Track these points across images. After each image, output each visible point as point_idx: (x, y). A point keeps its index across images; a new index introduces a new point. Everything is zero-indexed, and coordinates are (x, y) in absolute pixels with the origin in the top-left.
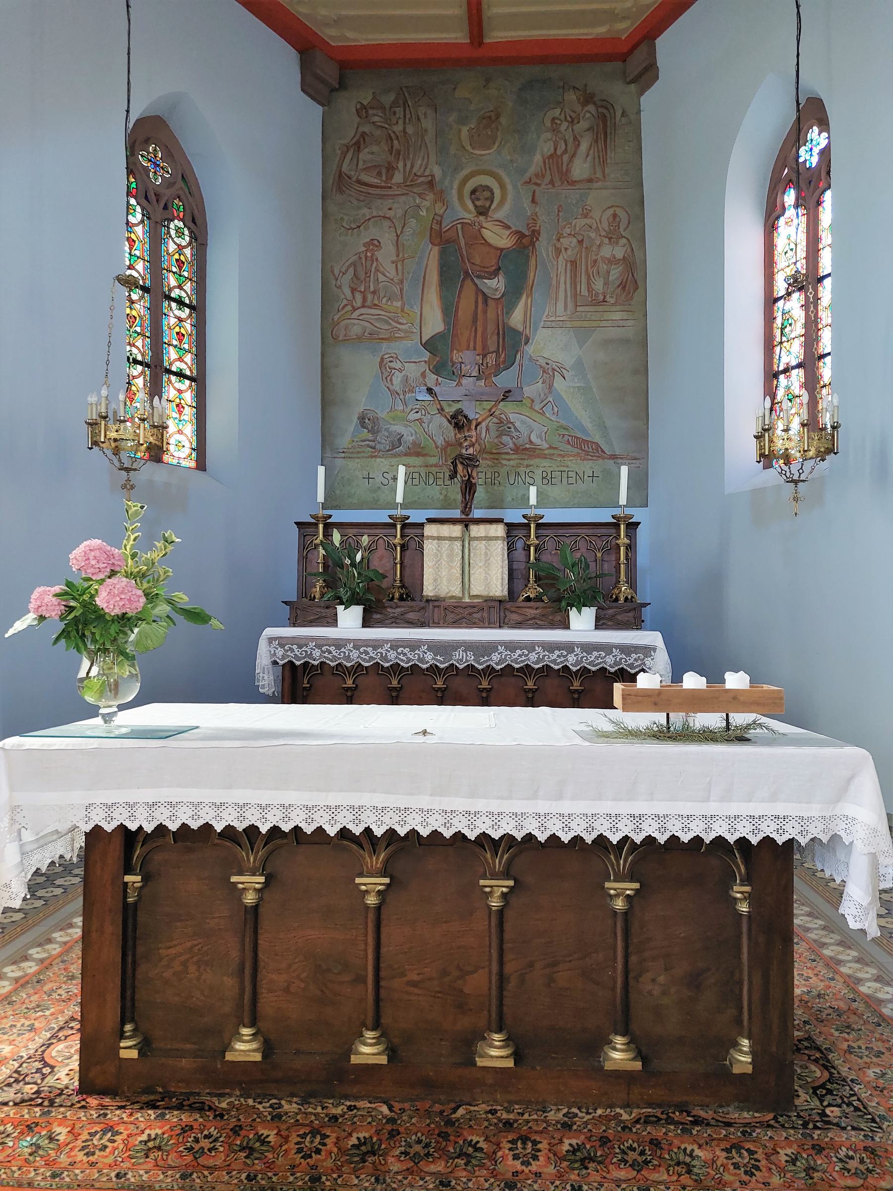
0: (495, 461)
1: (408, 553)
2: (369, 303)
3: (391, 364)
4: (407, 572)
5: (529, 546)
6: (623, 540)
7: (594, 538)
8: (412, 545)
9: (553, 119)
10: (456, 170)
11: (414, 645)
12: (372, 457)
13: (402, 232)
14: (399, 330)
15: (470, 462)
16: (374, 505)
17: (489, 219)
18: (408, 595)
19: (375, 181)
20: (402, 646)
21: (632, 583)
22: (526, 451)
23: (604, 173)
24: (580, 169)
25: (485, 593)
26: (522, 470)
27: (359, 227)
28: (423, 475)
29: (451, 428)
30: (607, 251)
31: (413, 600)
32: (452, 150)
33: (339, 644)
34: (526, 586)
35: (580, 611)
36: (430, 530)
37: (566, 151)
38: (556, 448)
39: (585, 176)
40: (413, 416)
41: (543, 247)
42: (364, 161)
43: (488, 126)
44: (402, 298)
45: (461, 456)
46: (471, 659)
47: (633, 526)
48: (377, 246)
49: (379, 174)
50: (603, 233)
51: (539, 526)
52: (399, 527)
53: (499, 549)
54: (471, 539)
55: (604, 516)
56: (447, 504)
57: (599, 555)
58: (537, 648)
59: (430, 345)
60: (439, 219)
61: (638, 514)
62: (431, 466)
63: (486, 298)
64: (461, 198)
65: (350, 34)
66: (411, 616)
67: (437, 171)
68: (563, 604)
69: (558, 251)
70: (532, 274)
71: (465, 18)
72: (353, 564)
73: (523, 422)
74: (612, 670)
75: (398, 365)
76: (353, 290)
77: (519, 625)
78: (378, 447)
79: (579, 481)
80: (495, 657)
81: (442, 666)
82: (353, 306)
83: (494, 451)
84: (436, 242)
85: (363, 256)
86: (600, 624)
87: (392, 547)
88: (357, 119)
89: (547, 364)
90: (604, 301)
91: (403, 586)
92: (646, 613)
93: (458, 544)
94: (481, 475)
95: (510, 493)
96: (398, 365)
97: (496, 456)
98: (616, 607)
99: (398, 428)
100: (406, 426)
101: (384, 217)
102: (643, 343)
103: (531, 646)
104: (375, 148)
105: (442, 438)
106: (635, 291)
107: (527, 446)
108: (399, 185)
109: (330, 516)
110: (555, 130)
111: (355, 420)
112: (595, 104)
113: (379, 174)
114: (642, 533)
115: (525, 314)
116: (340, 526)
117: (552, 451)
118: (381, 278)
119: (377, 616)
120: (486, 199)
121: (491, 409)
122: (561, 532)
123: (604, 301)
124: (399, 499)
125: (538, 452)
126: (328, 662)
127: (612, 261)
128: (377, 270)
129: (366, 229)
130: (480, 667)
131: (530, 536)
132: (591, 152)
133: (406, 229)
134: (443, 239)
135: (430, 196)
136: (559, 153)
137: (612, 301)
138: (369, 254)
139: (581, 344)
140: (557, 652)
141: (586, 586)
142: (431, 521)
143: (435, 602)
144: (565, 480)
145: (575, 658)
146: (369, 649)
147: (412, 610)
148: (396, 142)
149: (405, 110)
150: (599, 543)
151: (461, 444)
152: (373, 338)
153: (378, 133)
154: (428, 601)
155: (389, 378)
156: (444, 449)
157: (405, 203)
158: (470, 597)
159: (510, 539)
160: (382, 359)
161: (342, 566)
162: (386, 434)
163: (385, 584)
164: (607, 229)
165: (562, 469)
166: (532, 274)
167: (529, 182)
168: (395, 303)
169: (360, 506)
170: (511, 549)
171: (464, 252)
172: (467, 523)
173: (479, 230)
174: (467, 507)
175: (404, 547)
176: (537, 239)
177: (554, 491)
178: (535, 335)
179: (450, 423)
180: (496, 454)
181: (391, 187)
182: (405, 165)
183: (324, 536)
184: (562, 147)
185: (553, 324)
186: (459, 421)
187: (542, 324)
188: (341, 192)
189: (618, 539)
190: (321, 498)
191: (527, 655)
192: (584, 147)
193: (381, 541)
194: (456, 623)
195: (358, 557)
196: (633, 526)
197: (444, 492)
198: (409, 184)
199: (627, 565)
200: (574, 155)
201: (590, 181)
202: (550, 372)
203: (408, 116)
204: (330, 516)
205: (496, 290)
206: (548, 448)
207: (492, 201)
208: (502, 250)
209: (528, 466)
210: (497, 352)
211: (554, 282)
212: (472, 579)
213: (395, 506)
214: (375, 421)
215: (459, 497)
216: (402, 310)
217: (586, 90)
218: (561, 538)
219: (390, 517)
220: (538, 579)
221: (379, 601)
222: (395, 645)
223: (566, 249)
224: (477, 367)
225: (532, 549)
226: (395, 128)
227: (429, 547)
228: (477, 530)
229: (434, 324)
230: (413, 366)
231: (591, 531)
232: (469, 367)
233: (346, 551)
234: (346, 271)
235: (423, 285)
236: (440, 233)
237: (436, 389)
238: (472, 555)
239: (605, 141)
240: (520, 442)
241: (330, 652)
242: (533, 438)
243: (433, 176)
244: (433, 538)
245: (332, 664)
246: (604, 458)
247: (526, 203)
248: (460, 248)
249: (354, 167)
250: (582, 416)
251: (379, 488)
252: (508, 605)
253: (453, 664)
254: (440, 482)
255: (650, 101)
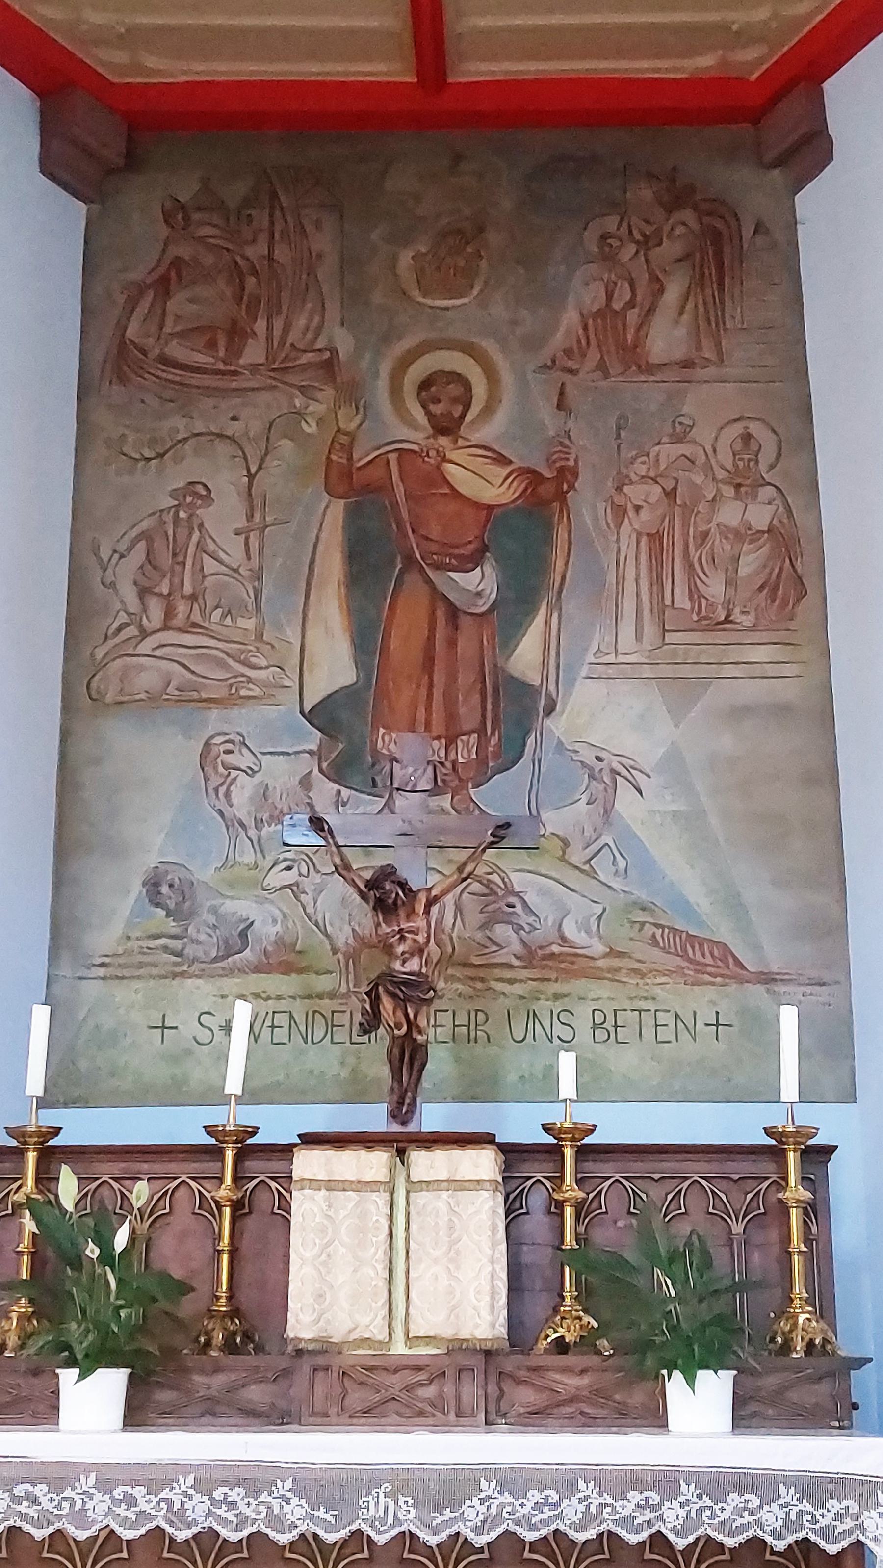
0: (479, 985)
1: (250, 1224)
2: (179, 620)
3: (229, 758)
4: (248, 1273)
5: (560, 1205)
6: (796, 1192)
7: (724, 1184)
8: (263, 1200)
9: (604, 237)
10: (387, 339)
11: (254, 1479)
12: (175, 976)
13: (260, 468)
14: (250, 680)
15: (413, 992)
16: (175, 1094)
17: (461, 442)
18: (247, 1337)
19: (201, 359)
20: (224, 1483)
21: (824, 1306)
22: (552, 961)
23: (718, 345)
24: (666, 338)
25: (448, 1332)
26: (543, 1007)
27: (161, 456)
28: (300, 1018)
29: (367, 908)
30: (730, 514)
31: (259, 1349)
32: (377, 298)
33: (59, 1476)
34: (556, 1311)
35: (691, 1381)
36: (308, 1164)
37: (631, 304)
38: (621, 955)
39: (679, 354)
40: (278, 878)
41: (587, 505)
42: (178, 317)
43: (458, 251)
44: (258, 609)
45: (388, 976)
46: (408, 1517)
47: (818, 1156)
48: (201, 497)
49: (212, 345)
50: (721, 474)
51: (585, 1152)
52: (229, 1155)
53: (486, 1211)
54: (413, 1186)
55: (744, 1125)
56: (356, 1092)
57: (738, 1228)
58: (582, 1485)
59: (324, 716)
60: (344, 439)
61: (827, 1123)
62: (320, 997)
63: (454, 613)
64: (396, 391)
65: (151, 62)
66: (256, 1394)
67: (345, 343)
68: (650, 1362)
69: (620, 513)
70: (560, 564)
71: (407, 38)
72: (107, 1257)
73: (542, 892)
74: (780, 1546)
75: (244, 760)
76: (143, 592)
77: (537, 1418)
78: (189, 951)
79: (685, 1036)
80: (473, 1511)
81: (331, 1538)
82: (141, 627)
83: (477, 961)
84: (341, 490)
85: (169, 518)
86: (747, 1413)
87: (208, 1208)
88: (164, 231)
89: (598, 759)
90: (727, 620)
91: (235, 1313)
92: (864, 1384)
93: (381, 1199)
94: (445, 1019)
95: (516, 1062)
96: (244, 760)
97: (482, 973)
98: (785, 1369)
99: (241, 907)
100: (261, 901)
101: (220, 436)
102: (825, 716)
103: (566, 1481)
104: (202, 291)
105: (347, 930)
106: (798, 600)
107: (555, 949)
108: (254, 368)
109: (57, 1131)
110: (608, 257)
111: (137, 888)
112: (695, 208)
113: (212, 345)
114: (841, 1174)
115: (546, 647)
116: (78, 1155)
117: (616, 962)
118: (210, 565)
119: (164, 1396)
120: (455, 400)
121: (465, 864)
122: (638, 1167)
123: (727, 620)
124: (234, 1085)
125: (582, 962)
126: (27, 1527)
127: (742, 535)
128: (201, 547)
129: (179, 460)
130: (433, 1541)
131: (562, 1178)
132: (690, 306)
133: (272, 463)
134: (353, 483)
135: (328, 393)
136: (617, 305)
137: (747, 621)
138: (182, 514)
139: (677, 712)
140: (635, 1497)
141: (705, 1312)
142: (311, 1140)
143: (320, 1356)
144: (648, 1033)
145: (682, 1513)
146: (139, 1492)
147: (256, 1376)
148: (251, 281)
149: (271, 216)
150: (736, 1195)
151: (388, 950)
152: (190, 699)
153: (209, 260)
154: (299, 1353)
155: (222, 790)
156: (352, 956)
157: (268, 406)
158: (410, 1340)
159: (514, 1183)
160: (207, 744)
161: (77, 1261)
162: (212, 920)
163: (187, 1307)
164: (729, 466)
165: (643, 1005)
166: (560, 564)
167: (550, 366)
168: (242, 623)
169: (142, 1096)
170: (514, 1211)
171: (405, 515)
172: (401, 1145)
173: (438, 467)
174: (403, 1109)
175: (237, 1206)
176: (572, 487)
177: (625, 1060)
178: (568, 694)
179: (363, 896)
180: (477, 968)
181: (235, 373)
182: (270, 328)
183: (38, 1180)
184: (623, 294)
185: (611, 671)
186: (386, 894)
187: (584, 672)
188: (123, 380)
189: (784, 1189)
190: (35, 1085)
191: (556, 1505)
192: (673, 293)
193: (182, 1192)
194: (371, 1415)
195: (121, 1240)
196: (818, 1156)
197: (351, 1060)
198: (279, 368)
199: (808, 1257)
200: (651, 311)
201: (687, 364)
202: (607, 777)
203: (278, 228)
204: (57, 1131)
205: (479, 594)
206: (606, 956)
207: (467, 407)
208: (490, 508)
209: (557, 997)
210: (481, 731)
211: (612, 578)
212: (413, 1294)
213: (224, 1100)
214: (185, 890)
215: (385, 1072)
216: (260, 636)
217: (673, 181)
218: (638, 1182)
219: (210, 1130)
220: (586, 1295)
221: (170, 1353)
222: (206, 1479)
223: (638, 509)
224: (430, 769)
225: (568, 1211)
226: (250, 251)
227: (304, 1207)
228: (425, 1163)
229: (333, 665)
230: (280, 758)
231: (714, 1166)
232: (411, 770)
233: (91, 1222)
234: (130, 549)
235: (309, 584)
236: (347, 473)
237: (331, 819)
238: (414, 1227)
239: (721, 284)
240: (544, 932)
241: (35, 1501)
242: (570, 930)
243: (334, 352)
244: (314, 1184)
245: (39, 1534)
246: (742, 981)
247: (549, 419)
248: (395, 505)
249: (153, 329)
250: (689, 884)
251: (189, 1052)
252: (509, 1364)
253: (359, 1532)
254: (341, 1035)
255: (816, 204)
